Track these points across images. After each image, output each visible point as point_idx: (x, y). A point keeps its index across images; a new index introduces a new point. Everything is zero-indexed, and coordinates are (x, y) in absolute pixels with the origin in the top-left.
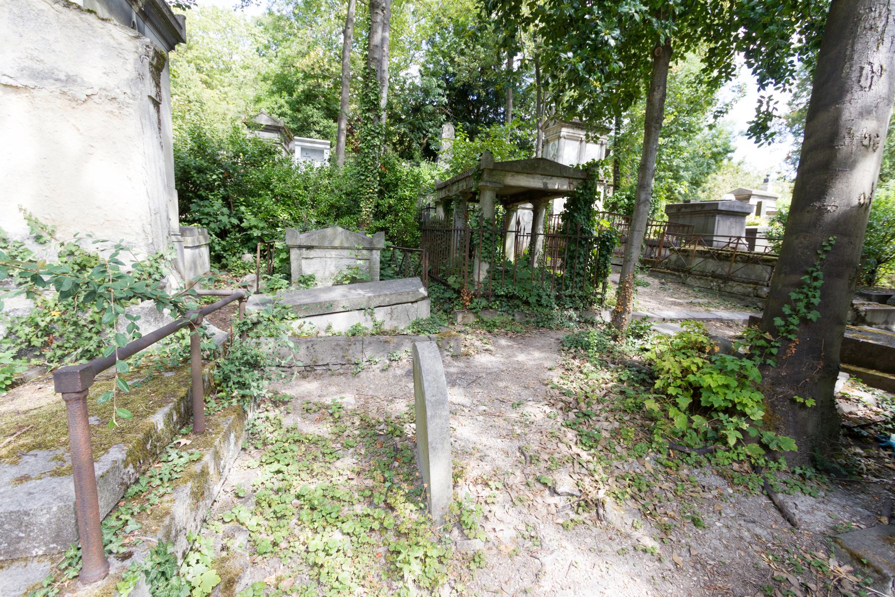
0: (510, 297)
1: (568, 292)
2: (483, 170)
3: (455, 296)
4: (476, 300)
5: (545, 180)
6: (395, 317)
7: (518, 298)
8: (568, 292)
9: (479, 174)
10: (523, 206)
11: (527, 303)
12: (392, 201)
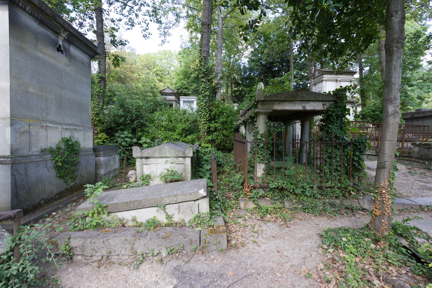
1: (329, 184)
4: (254, 191)
5: (303, 105)
6: (181, 211)
8: (329, 184)
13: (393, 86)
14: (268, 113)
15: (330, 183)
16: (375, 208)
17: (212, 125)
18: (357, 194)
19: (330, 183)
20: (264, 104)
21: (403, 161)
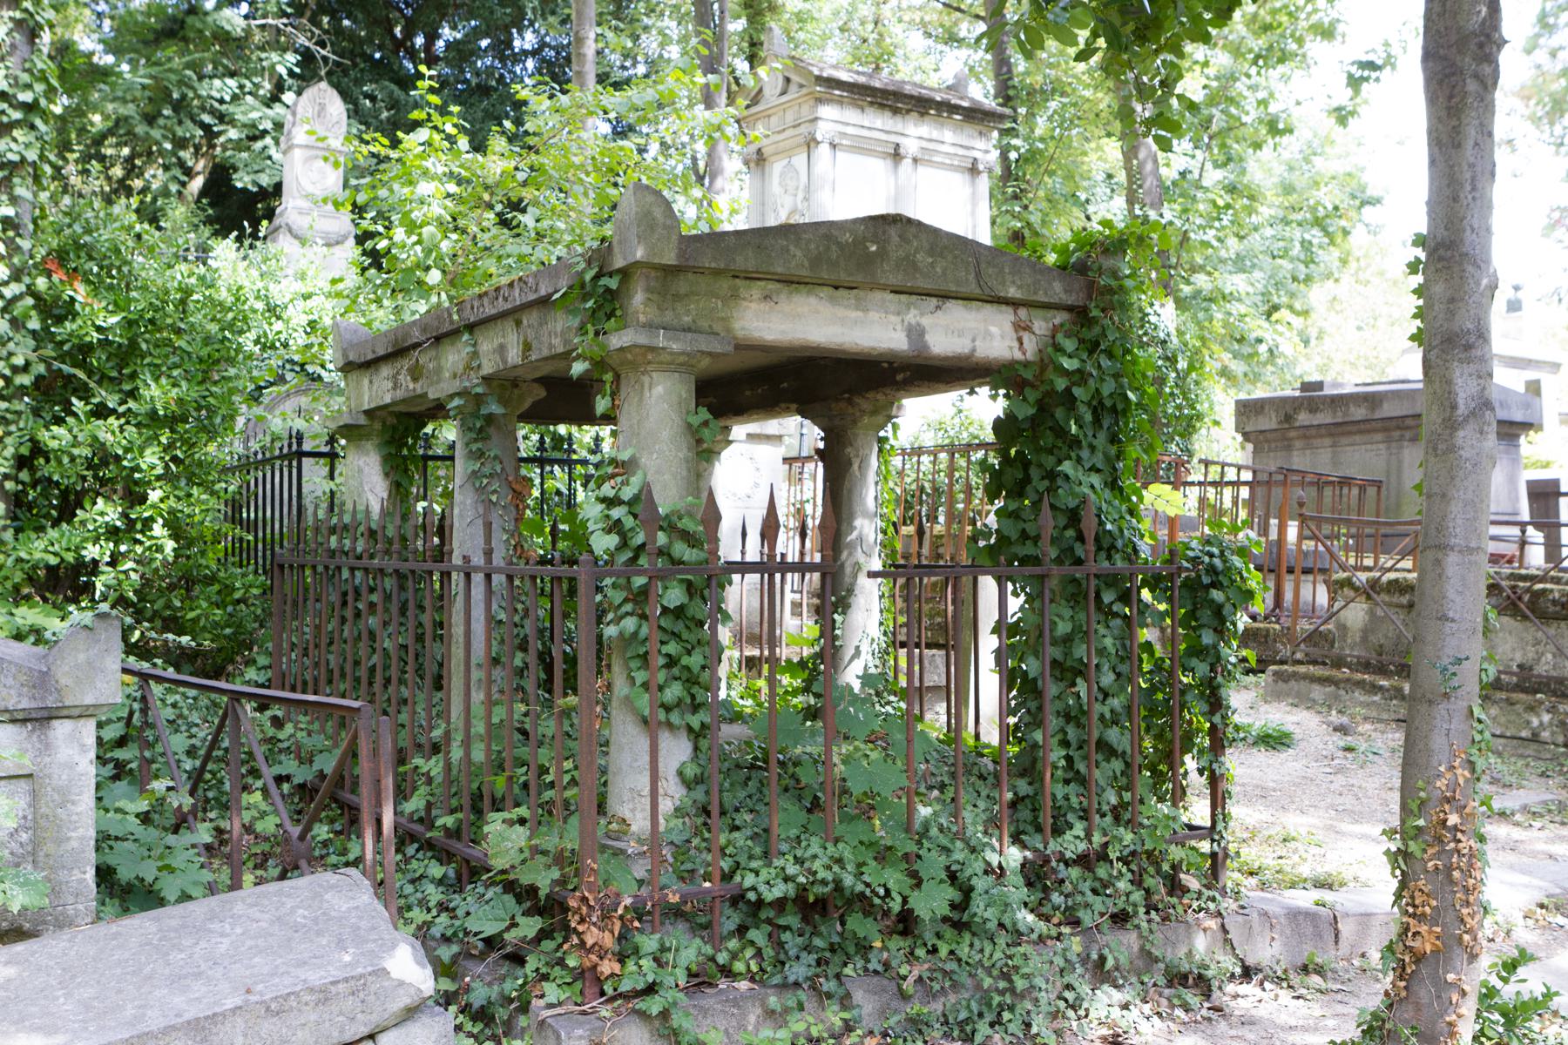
0: (813, 907)
1: (1073, 842)
2: (625, 273)
3: (530, 926)
4: (649, 943)
5: (912, 317)
7: (863, 903)
9: (601, 289)
10: (753, 427)
11: (906, 923)
12: (109, 432)
13: (1470, 268)
14: (705, 363)
15: (1079, 829)
16: (1414, 916)
17: (56, 437)
18: (1208, 887)
19: (1079, 829)
20: (677, 297)
21: (1303, 685)
